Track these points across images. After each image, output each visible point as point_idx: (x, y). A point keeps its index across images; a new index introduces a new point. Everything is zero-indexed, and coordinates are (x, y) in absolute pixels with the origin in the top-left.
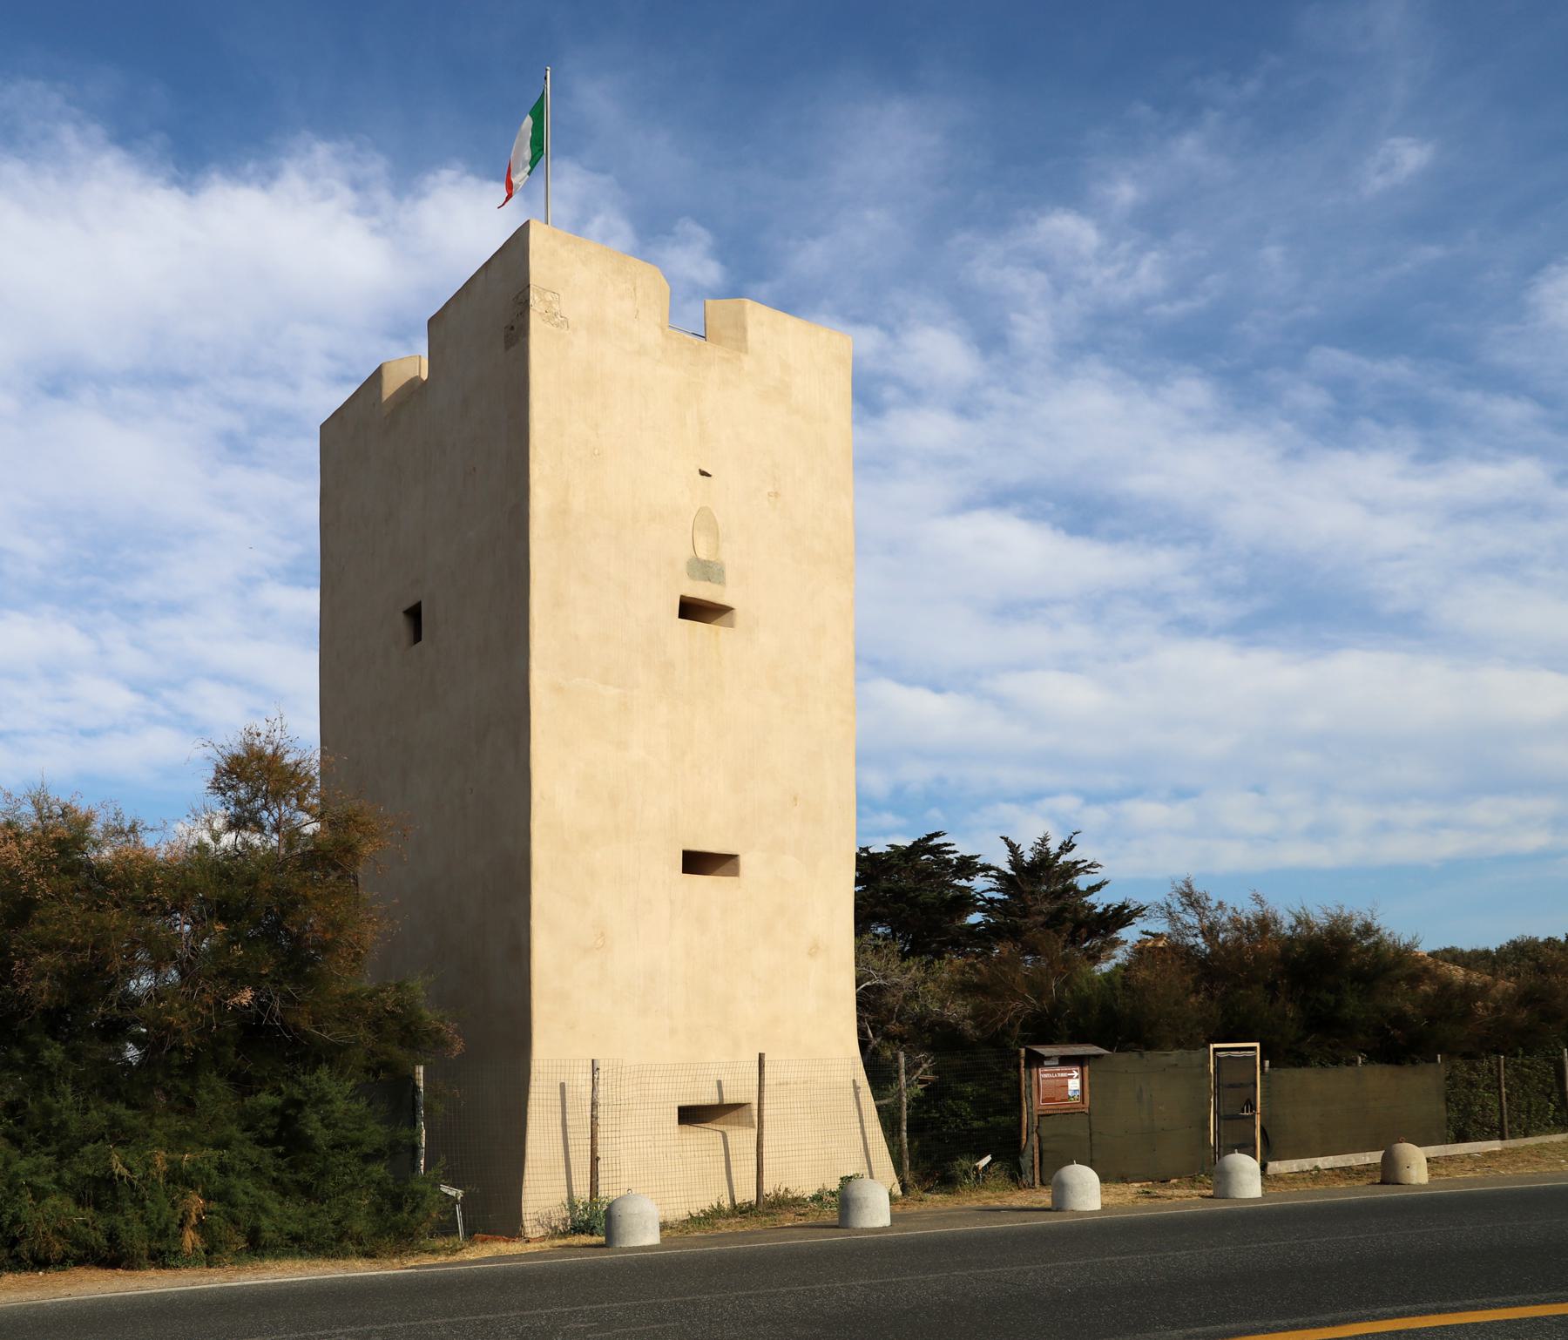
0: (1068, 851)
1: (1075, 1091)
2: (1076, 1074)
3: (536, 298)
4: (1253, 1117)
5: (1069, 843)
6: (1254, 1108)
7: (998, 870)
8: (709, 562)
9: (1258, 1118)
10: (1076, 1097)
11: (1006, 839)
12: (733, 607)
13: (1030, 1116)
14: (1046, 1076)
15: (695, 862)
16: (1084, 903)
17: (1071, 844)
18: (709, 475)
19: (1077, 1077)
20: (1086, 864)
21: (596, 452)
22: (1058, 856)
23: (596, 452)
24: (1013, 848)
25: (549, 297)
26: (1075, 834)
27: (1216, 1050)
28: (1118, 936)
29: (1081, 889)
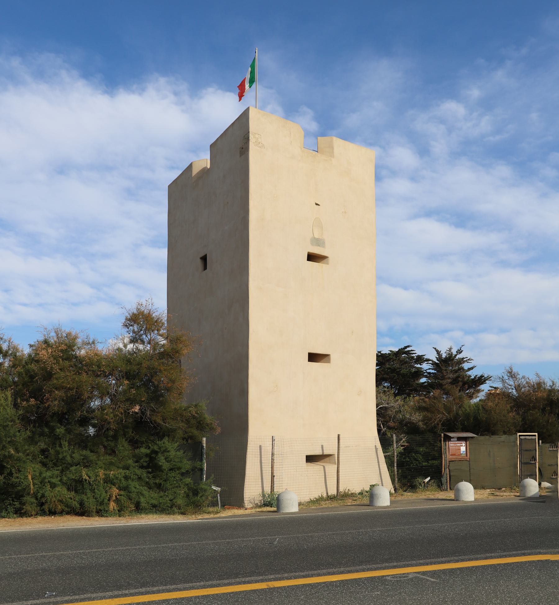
0: (460, 353)
3: (252, 136)
4: (535, 464)
5: (460, 350)
6: (535, 460)
8: (319, 239)
11: (435, 349)
12: (328, 256)
13: (445, 461)
14: (452, 445)
15: (313, 357)
17: (461, 351)
18: (319, 205)
19: (464, 446)
20: (467, 359)
21: (275, 196)
22: (456, 356)
23: (275, 196)
24: (438, 352)
25: (257, 136)
26: (462, 346)
27: (520, 436)
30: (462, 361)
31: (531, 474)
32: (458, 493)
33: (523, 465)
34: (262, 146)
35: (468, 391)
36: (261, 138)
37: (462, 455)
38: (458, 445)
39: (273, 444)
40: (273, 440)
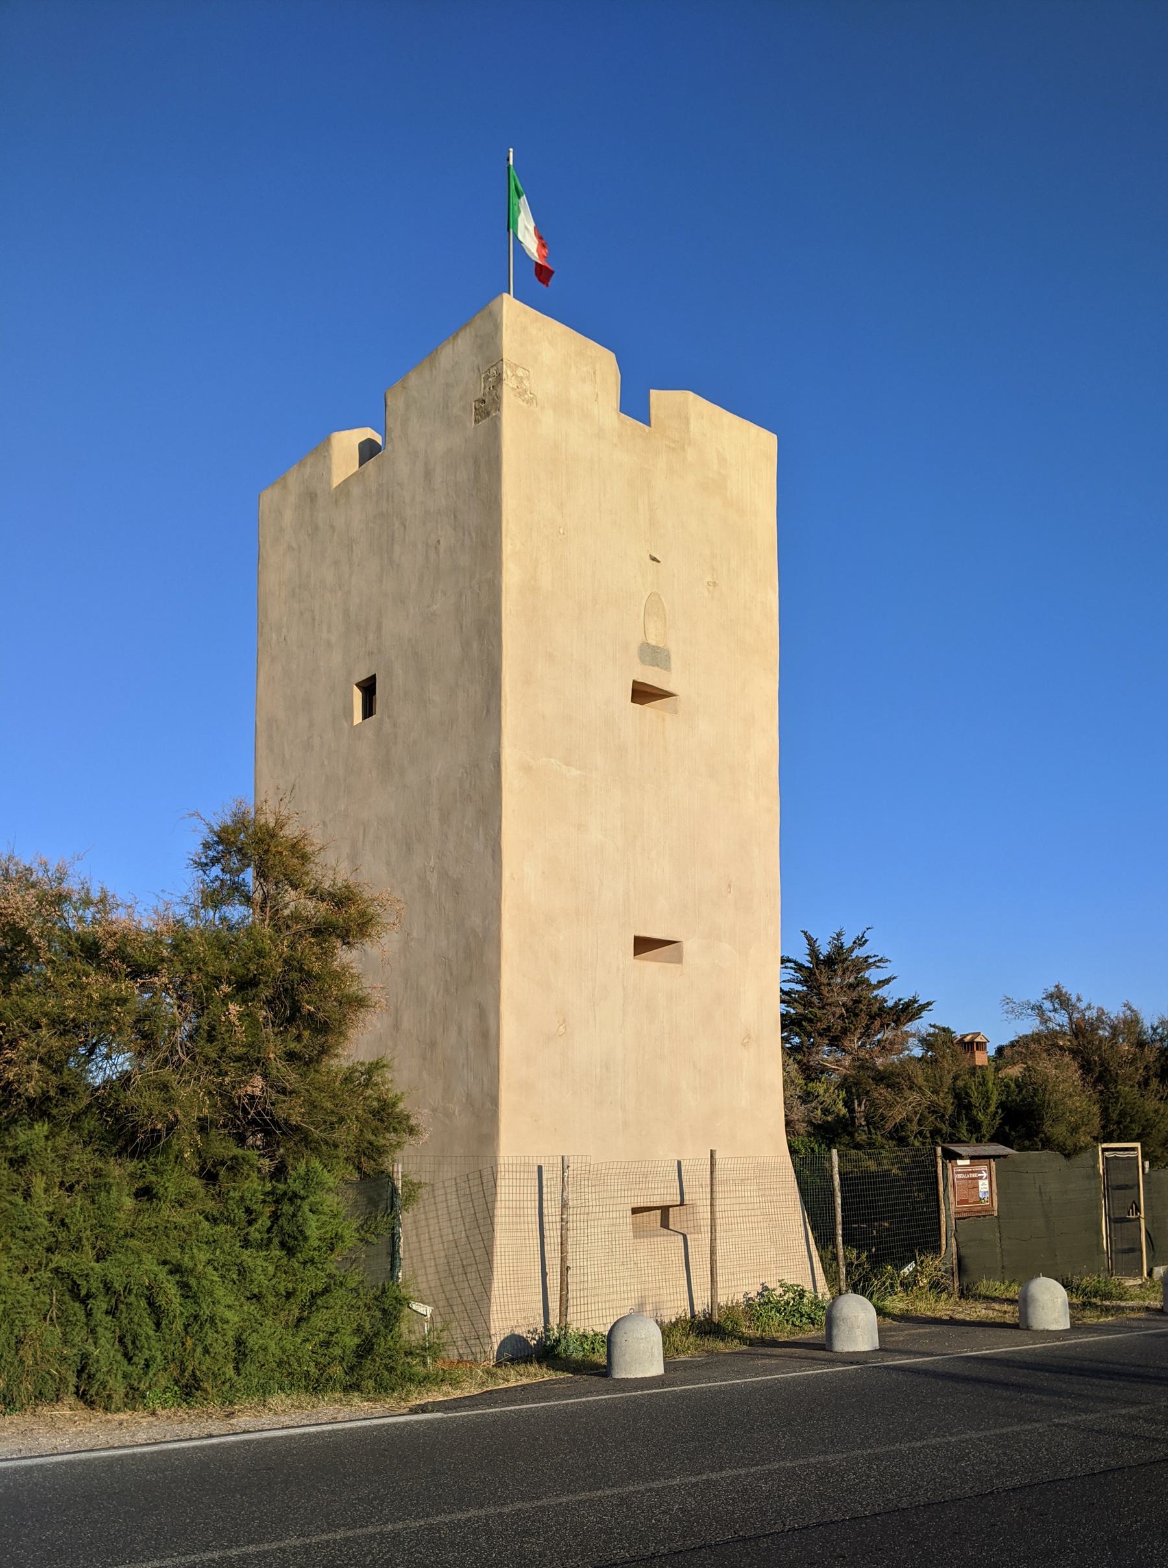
0: (861, 945)
1: (985, 1192)
3: (509, 372)
4: (1139, 1218)
5: (862, 938)
6: (1138, 1210)
7: (795, 962)
8: (658, 648)
9: (1142, 1221)
10: (986, 1199)
11: (805, 933)
12: (678, 693)
14: (959, 1176)
16: (876, 996)
17: (863, 939)
18: (658, 561)
19: (986, 1178)
20: (877, 959)
21: (562, 531)
22: (851, 950)
23: (562, 531)
24: (811, 942)
25: (520, 373)
26: (868, 929)
27: (1104, 1150)
28: (908, 1029)
29: (872, 983)
30: (865, 963)
31: (1130, 1246)
32: (1023, 1303)
33: (1113, 1225)
34: (531, 399)
35: (879, 1036)
36: (528, 378)
38: (974, 1175)
39: (566, 1179)
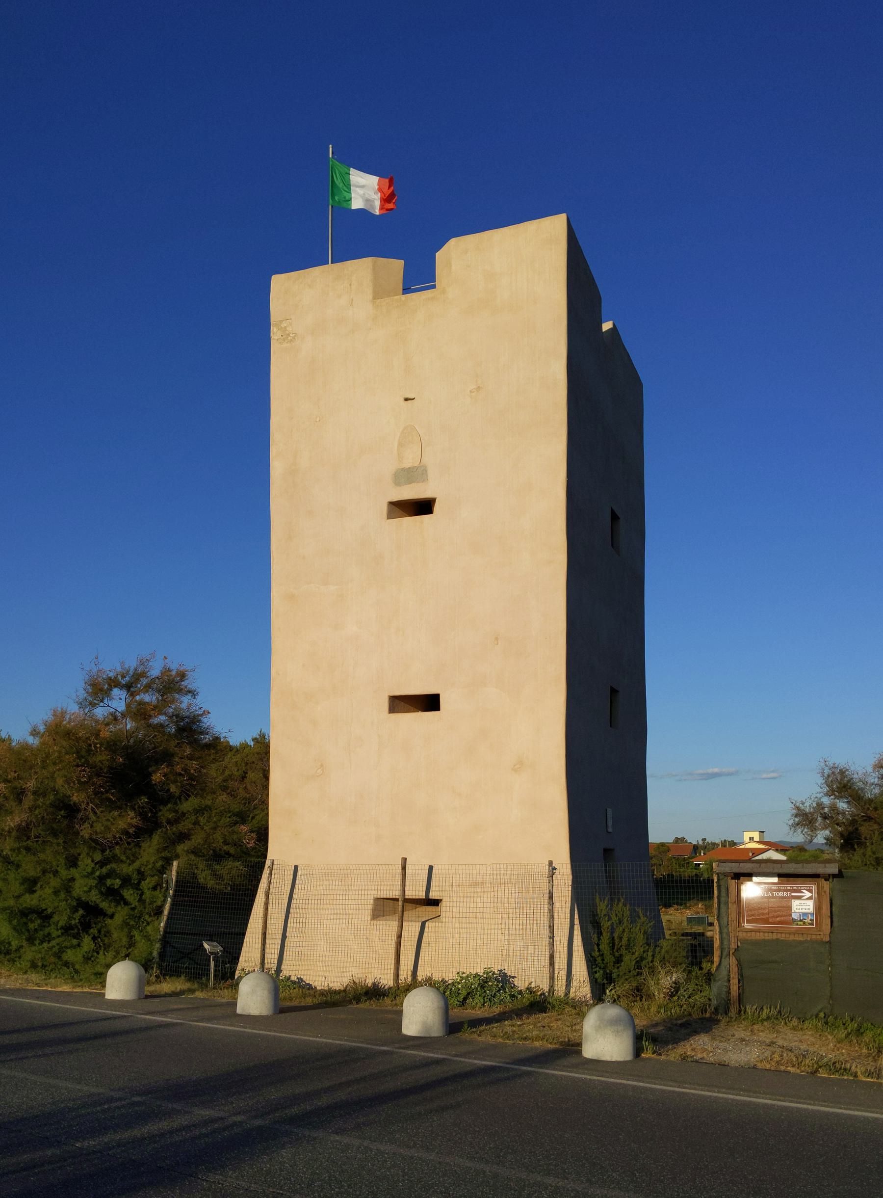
2: (808, 894)
23: (318, 420)
37: (801, 923)
40: (404, 868)
